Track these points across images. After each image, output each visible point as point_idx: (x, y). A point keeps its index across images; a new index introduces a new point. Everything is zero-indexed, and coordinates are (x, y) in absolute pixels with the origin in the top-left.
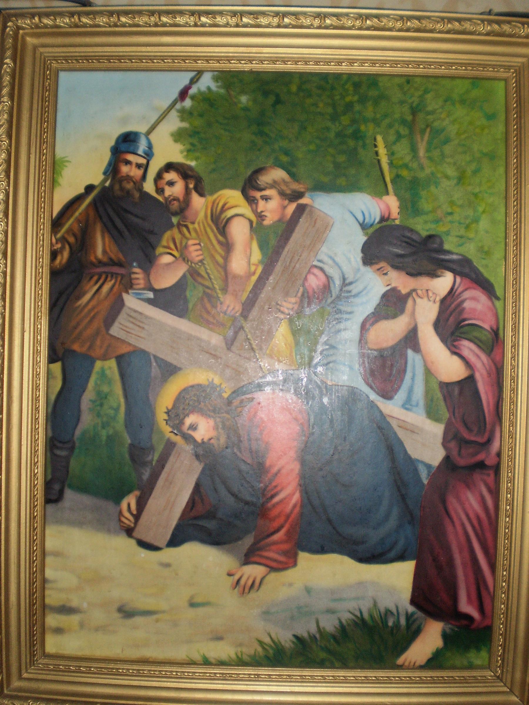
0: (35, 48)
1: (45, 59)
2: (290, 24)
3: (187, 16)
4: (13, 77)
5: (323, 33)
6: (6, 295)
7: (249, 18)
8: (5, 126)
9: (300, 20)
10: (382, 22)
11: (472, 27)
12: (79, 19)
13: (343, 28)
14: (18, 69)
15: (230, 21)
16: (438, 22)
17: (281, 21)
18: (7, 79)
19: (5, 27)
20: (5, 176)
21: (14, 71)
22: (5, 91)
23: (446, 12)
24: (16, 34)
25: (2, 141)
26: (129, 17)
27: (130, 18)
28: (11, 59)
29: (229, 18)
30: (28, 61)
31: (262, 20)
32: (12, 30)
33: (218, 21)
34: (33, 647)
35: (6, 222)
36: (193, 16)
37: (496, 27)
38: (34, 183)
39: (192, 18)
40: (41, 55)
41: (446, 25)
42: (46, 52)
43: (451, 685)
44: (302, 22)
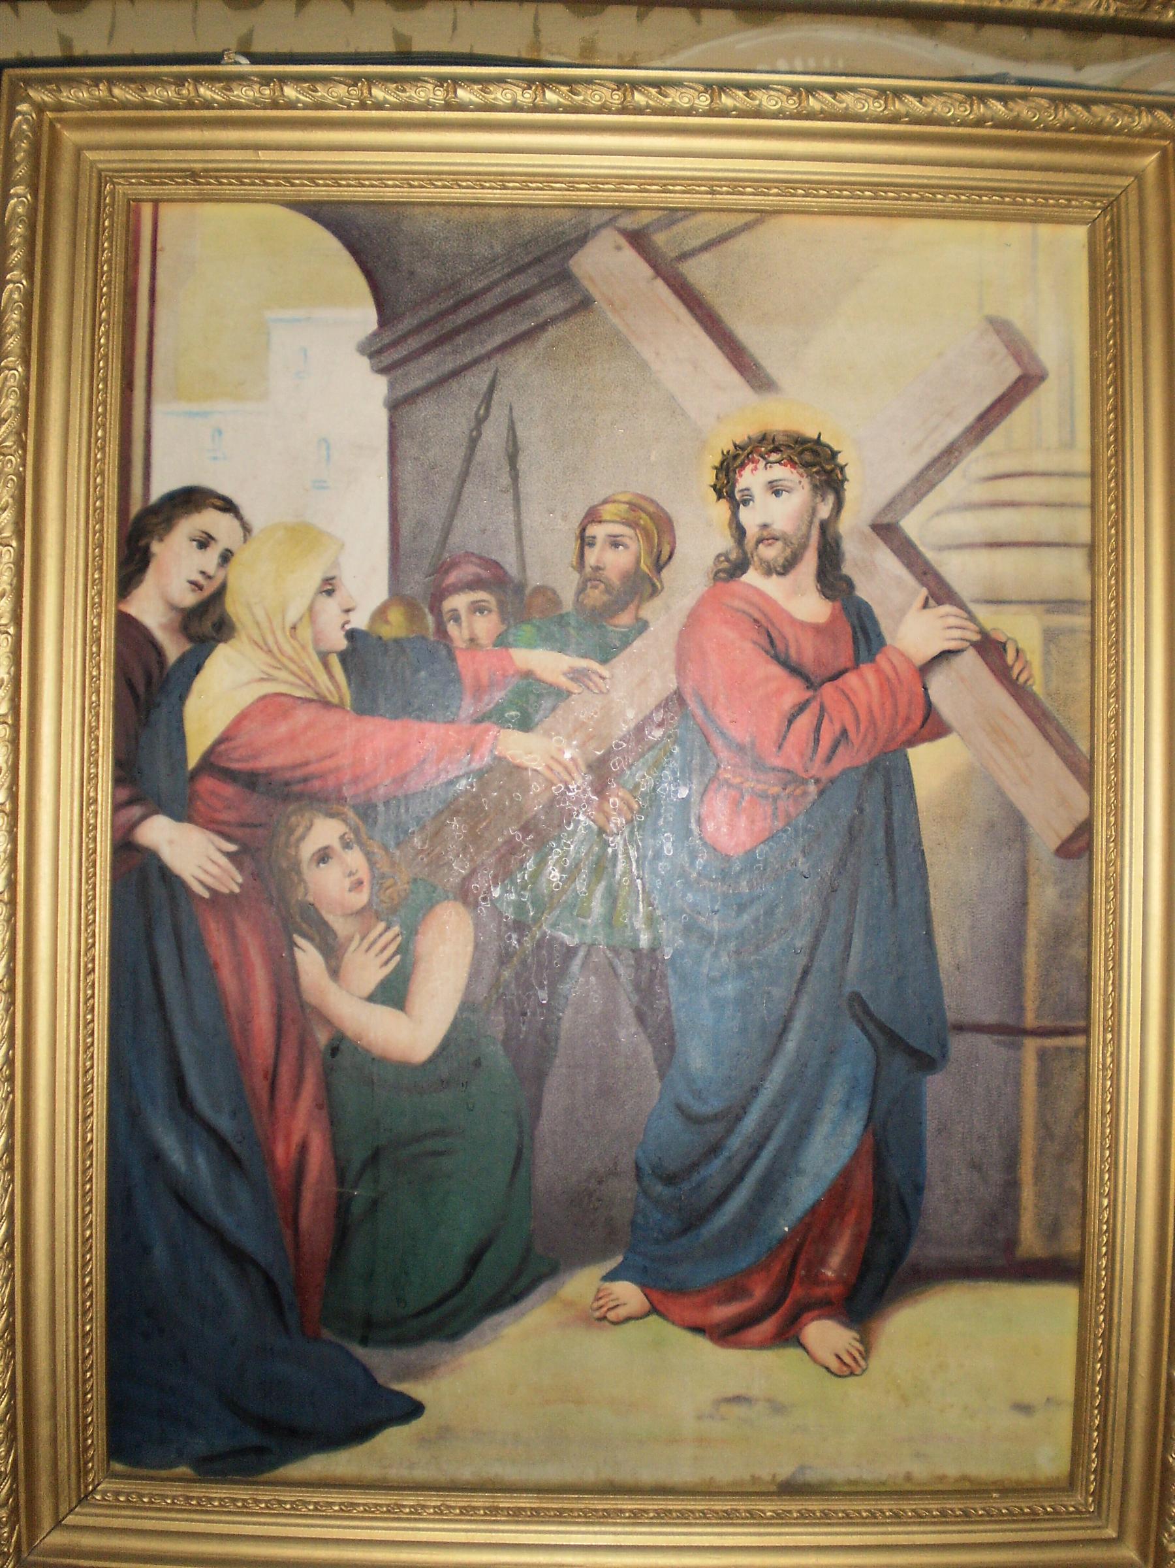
0: (79, 150)
1: (1099, 1514)
2: (560, 105)
3: (430, 87)
4: (32, 227)
5: (843, 129)
6: (19, 698)
7: (559, 94)
8: (13, 422)
9: (316, 91)
10: (841, 102)
11: (859, 106)
12: (110, 91)
13: (758, 114)
14: (41, 208)
15: (520, 98)
16: (876, 98)
17: (451, 95)
18: (14, 318)
19: (13, 113)
20: (13, 533)
21: (33, 210)
22: (16, 257)
23: (934, 79)
24: (37, 127)
25: (5, 455)
26: (302, 89)
27: (50, 91)
28: (28, 186)
29: (519, 91)
30: (64, 180)
31: (499, 96)
32: (27, 121)
33: (237, 96)
34: (84, 1408)
35: (20, 457)
36: (442, 86)
37: (998, 106)
38: (234, 1523)
39: (354, 92)
40: (91, 167)
41: (975, 107)
42: (101, 161)
43: (1005, 1526)
44: (673, 102)
